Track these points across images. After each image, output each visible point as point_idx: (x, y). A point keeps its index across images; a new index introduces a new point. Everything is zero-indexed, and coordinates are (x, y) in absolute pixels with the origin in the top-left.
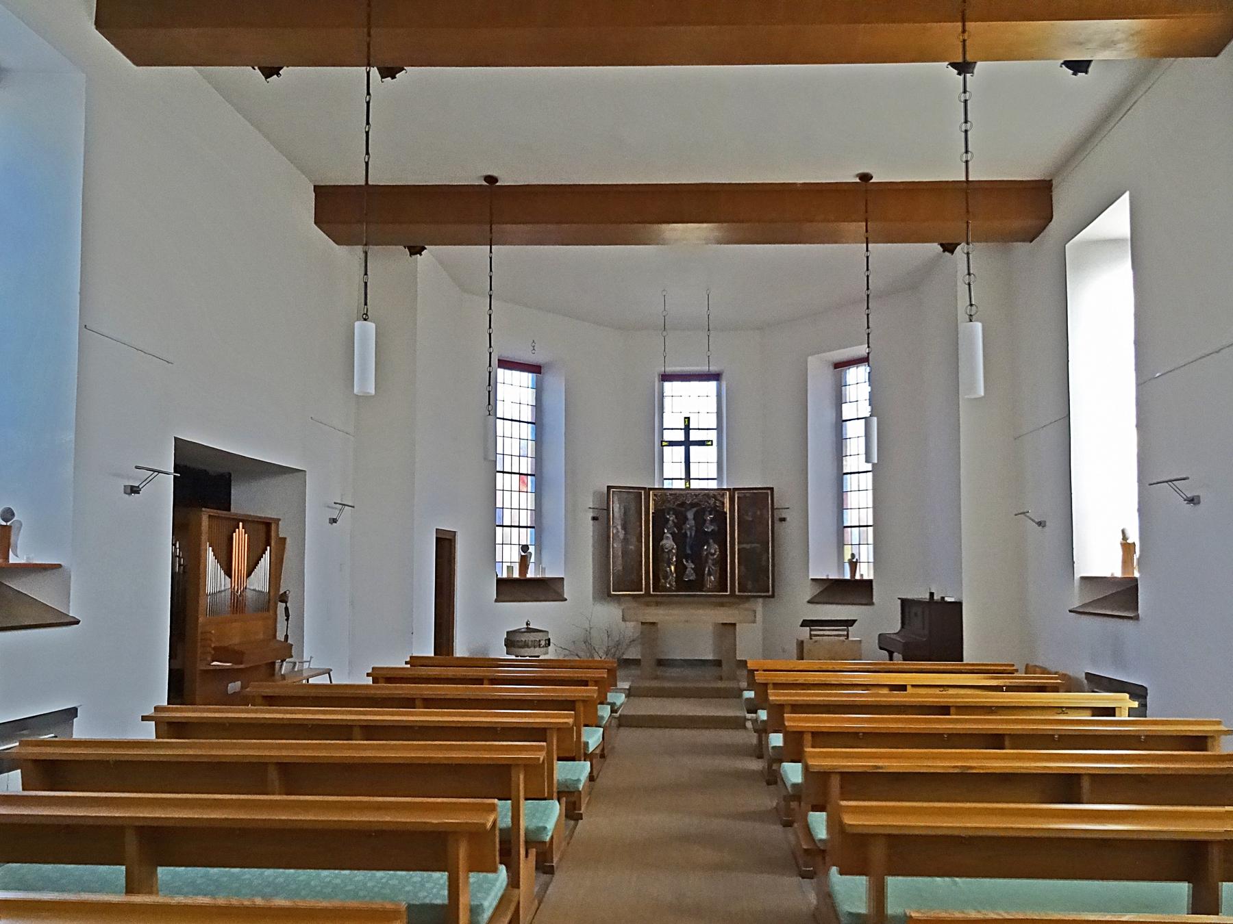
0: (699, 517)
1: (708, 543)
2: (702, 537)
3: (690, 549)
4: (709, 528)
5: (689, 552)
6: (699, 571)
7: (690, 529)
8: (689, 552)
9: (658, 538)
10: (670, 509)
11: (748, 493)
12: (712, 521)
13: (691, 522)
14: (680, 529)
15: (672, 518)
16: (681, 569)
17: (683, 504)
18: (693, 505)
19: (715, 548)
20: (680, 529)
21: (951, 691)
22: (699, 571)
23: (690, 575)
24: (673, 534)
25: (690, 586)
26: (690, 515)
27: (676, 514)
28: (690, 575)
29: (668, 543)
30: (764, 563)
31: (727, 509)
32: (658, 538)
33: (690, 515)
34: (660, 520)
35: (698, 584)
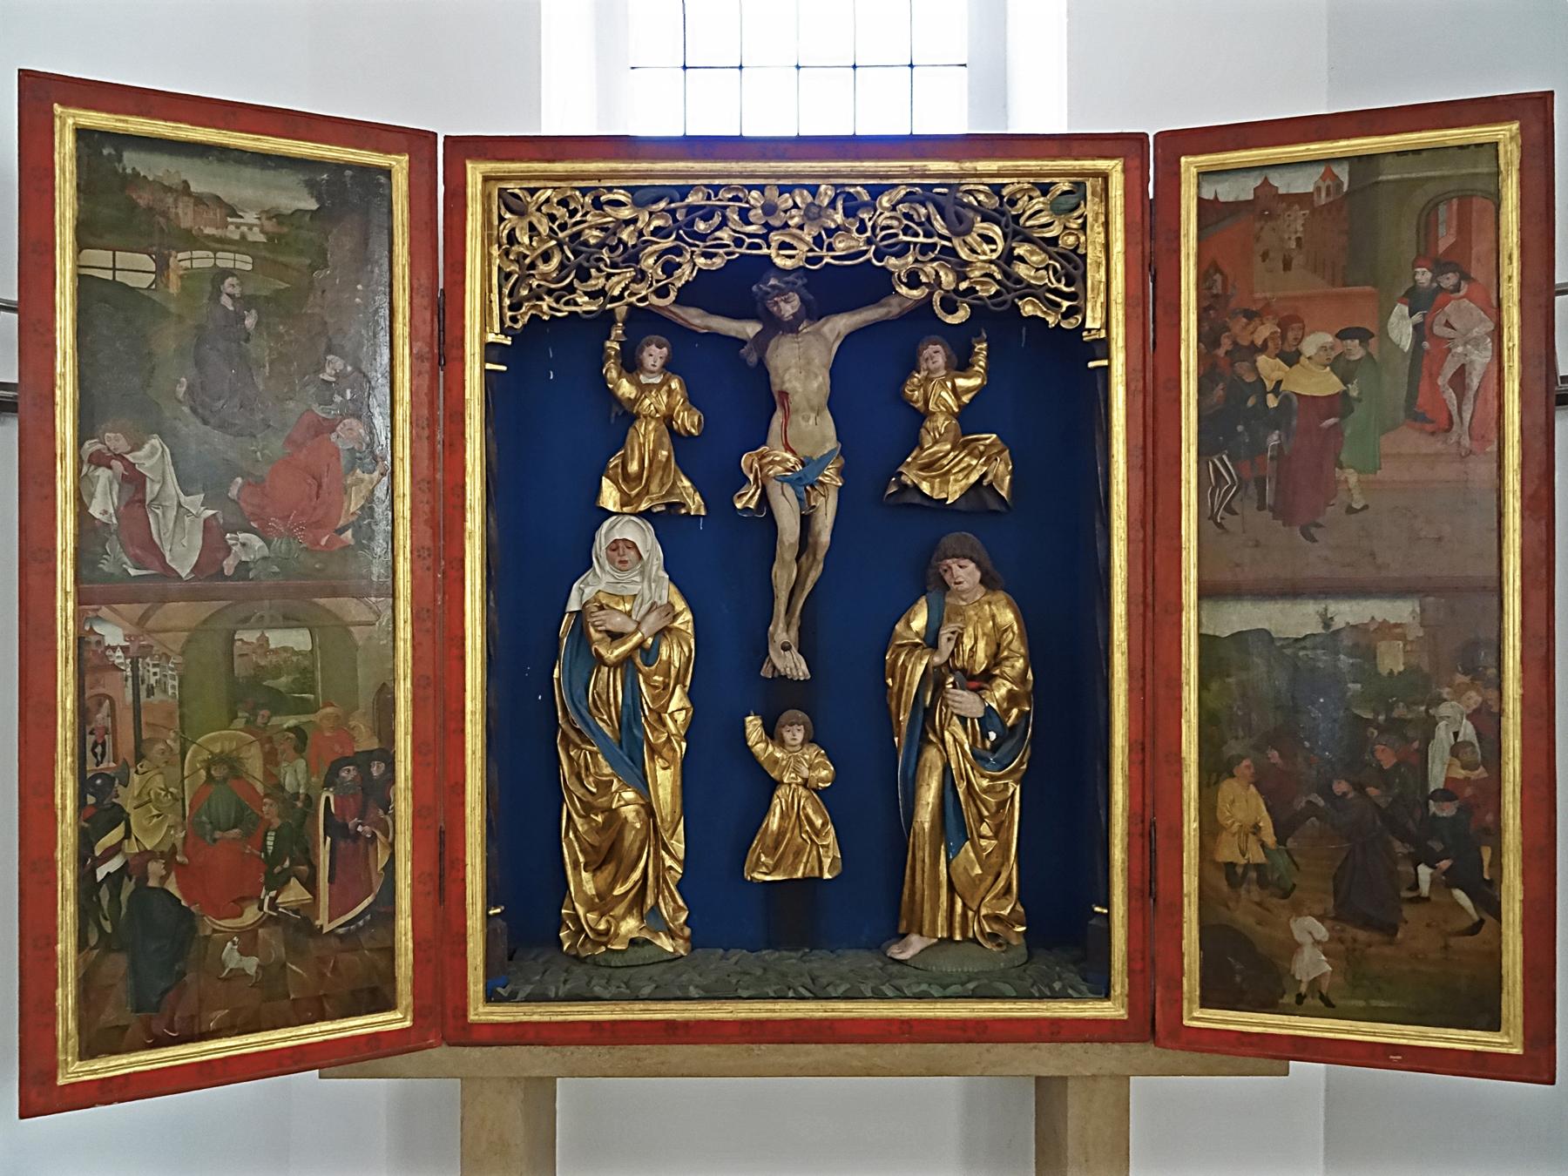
0: (873, 411)
1: (931, 584)
2: (892, 541)
3: (802, 646)
4: (952, 470)
5: (794, 665)
6: (870, 801)
7: (804, 482)
8: (794, 665)
9: (541, 546)
10: (644, 322)
11: (1299, 170)
12: (970, 419)
13: (807, 430)
14: (720, 480)
15: (655, 395)
16: (726, 793)
17: (738, 286)
18: (831, 288)
19: (986, 624)
20: (720, 480)
21: (386, 351)
22: (870, 801)
23: (800, 836)
24: (665, 521)
25: (794, 928)
26: (802, 366)
27: (695, 359)
28: (800, 836)
29: (629, 589)
30: (377, 570)
31: (1107, 311)
32: (541, 546)
33: (802, 366)
34: (551, 394)
35: (849, 918)
